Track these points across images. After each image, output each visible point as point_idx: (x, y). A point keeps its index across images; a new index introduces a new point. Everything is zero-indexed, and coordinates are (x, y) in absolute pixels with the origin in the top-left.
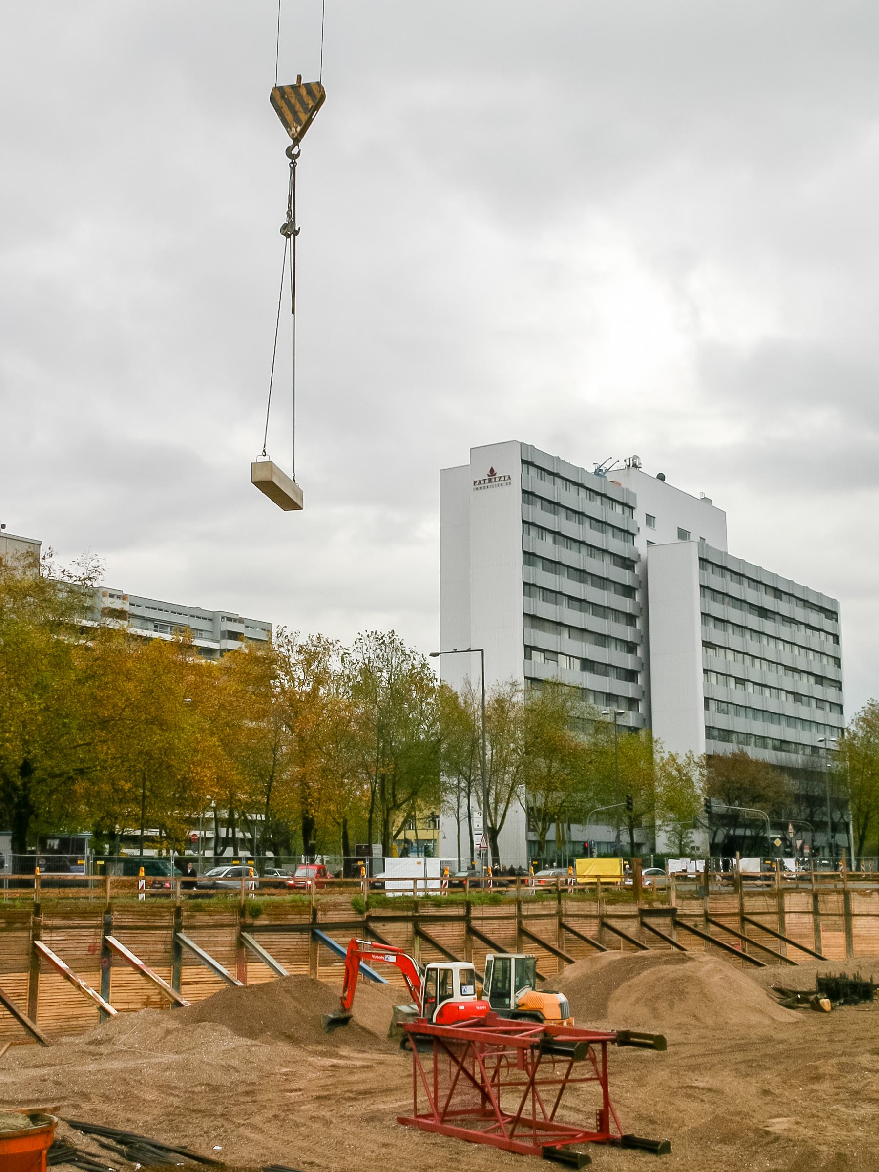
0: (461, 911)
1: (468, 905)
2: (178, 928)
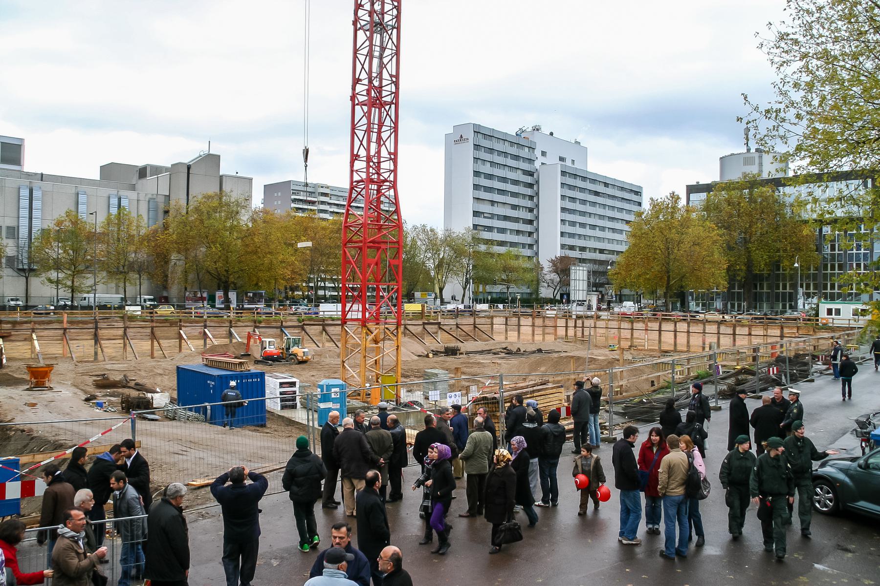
2: (231, 327)
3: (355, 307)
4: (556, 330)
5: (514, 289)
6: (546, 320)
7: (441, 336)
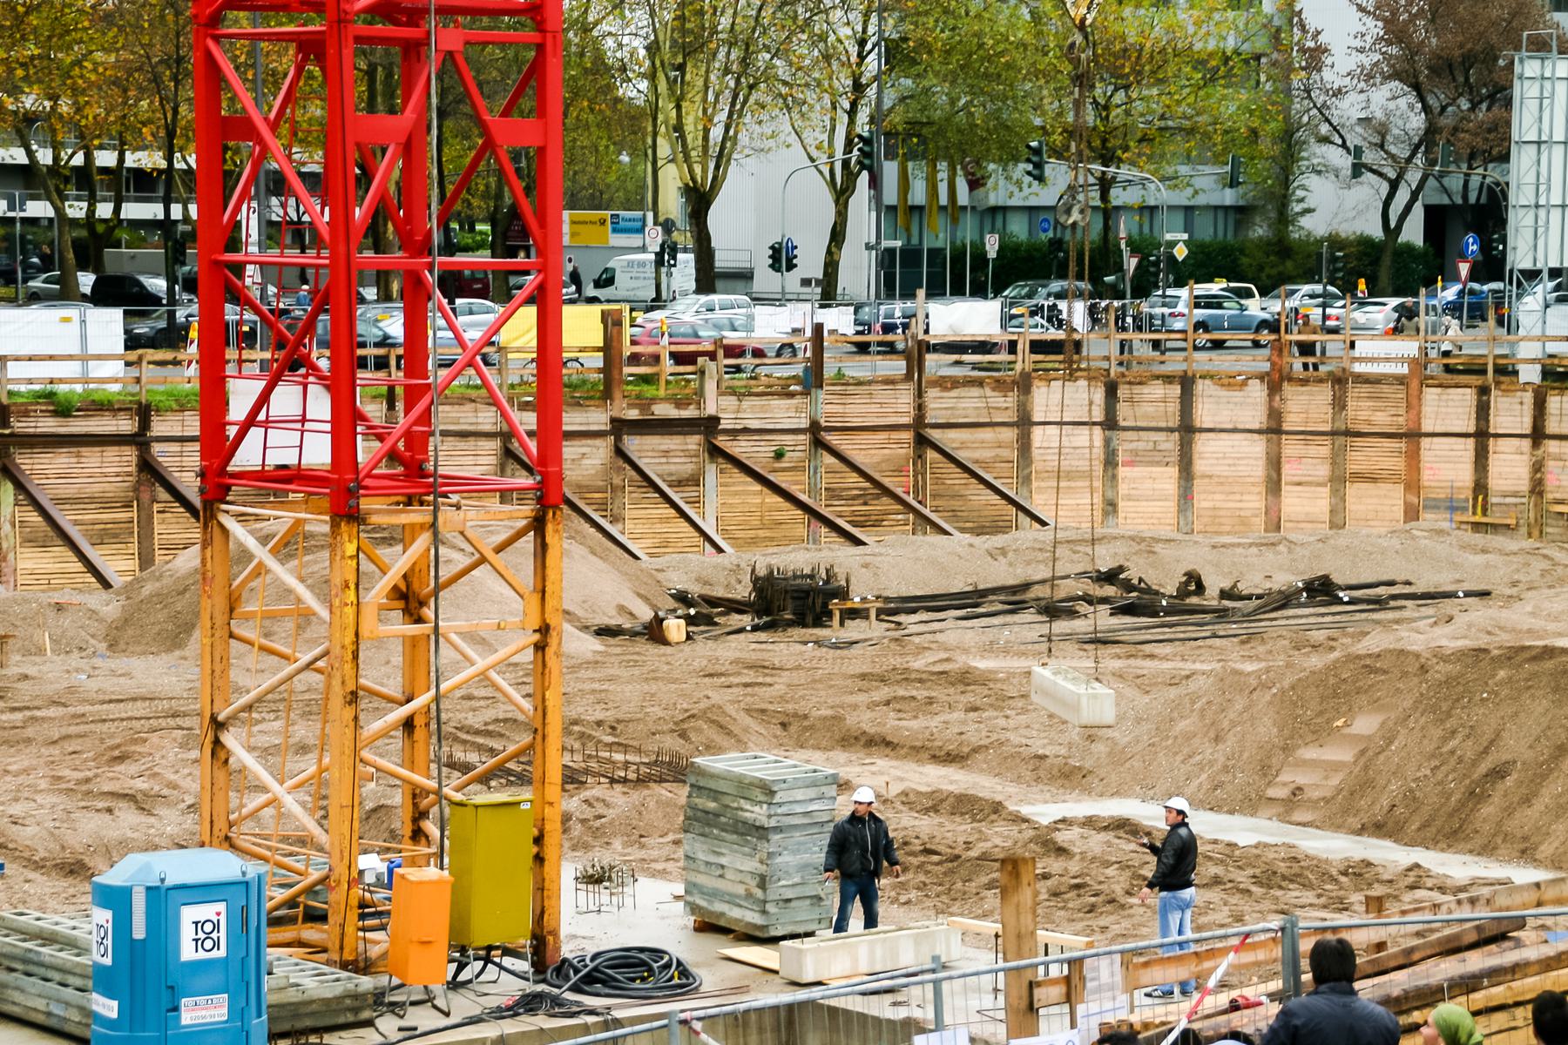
0: (126, 425)
1: (144, 413)
3: (285, 400)
4: (1413, 457)
5: (1138, 186)
6: (1354, 392)
7: (722, 499)
